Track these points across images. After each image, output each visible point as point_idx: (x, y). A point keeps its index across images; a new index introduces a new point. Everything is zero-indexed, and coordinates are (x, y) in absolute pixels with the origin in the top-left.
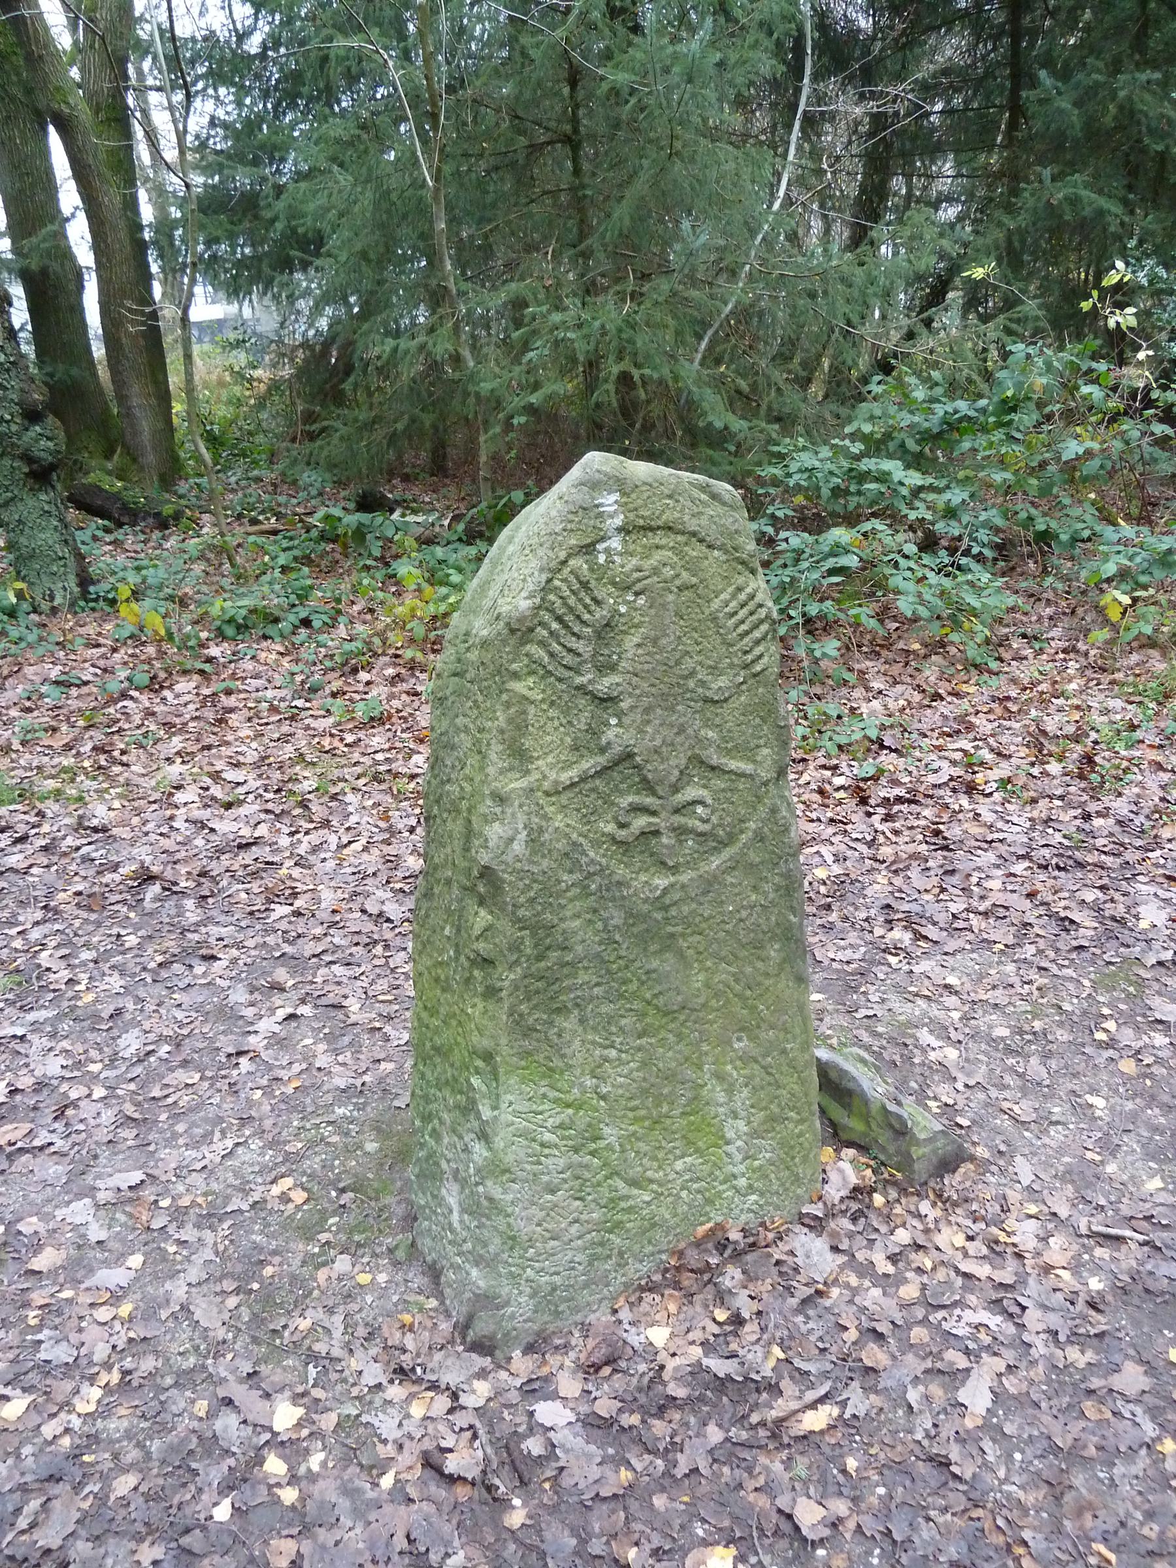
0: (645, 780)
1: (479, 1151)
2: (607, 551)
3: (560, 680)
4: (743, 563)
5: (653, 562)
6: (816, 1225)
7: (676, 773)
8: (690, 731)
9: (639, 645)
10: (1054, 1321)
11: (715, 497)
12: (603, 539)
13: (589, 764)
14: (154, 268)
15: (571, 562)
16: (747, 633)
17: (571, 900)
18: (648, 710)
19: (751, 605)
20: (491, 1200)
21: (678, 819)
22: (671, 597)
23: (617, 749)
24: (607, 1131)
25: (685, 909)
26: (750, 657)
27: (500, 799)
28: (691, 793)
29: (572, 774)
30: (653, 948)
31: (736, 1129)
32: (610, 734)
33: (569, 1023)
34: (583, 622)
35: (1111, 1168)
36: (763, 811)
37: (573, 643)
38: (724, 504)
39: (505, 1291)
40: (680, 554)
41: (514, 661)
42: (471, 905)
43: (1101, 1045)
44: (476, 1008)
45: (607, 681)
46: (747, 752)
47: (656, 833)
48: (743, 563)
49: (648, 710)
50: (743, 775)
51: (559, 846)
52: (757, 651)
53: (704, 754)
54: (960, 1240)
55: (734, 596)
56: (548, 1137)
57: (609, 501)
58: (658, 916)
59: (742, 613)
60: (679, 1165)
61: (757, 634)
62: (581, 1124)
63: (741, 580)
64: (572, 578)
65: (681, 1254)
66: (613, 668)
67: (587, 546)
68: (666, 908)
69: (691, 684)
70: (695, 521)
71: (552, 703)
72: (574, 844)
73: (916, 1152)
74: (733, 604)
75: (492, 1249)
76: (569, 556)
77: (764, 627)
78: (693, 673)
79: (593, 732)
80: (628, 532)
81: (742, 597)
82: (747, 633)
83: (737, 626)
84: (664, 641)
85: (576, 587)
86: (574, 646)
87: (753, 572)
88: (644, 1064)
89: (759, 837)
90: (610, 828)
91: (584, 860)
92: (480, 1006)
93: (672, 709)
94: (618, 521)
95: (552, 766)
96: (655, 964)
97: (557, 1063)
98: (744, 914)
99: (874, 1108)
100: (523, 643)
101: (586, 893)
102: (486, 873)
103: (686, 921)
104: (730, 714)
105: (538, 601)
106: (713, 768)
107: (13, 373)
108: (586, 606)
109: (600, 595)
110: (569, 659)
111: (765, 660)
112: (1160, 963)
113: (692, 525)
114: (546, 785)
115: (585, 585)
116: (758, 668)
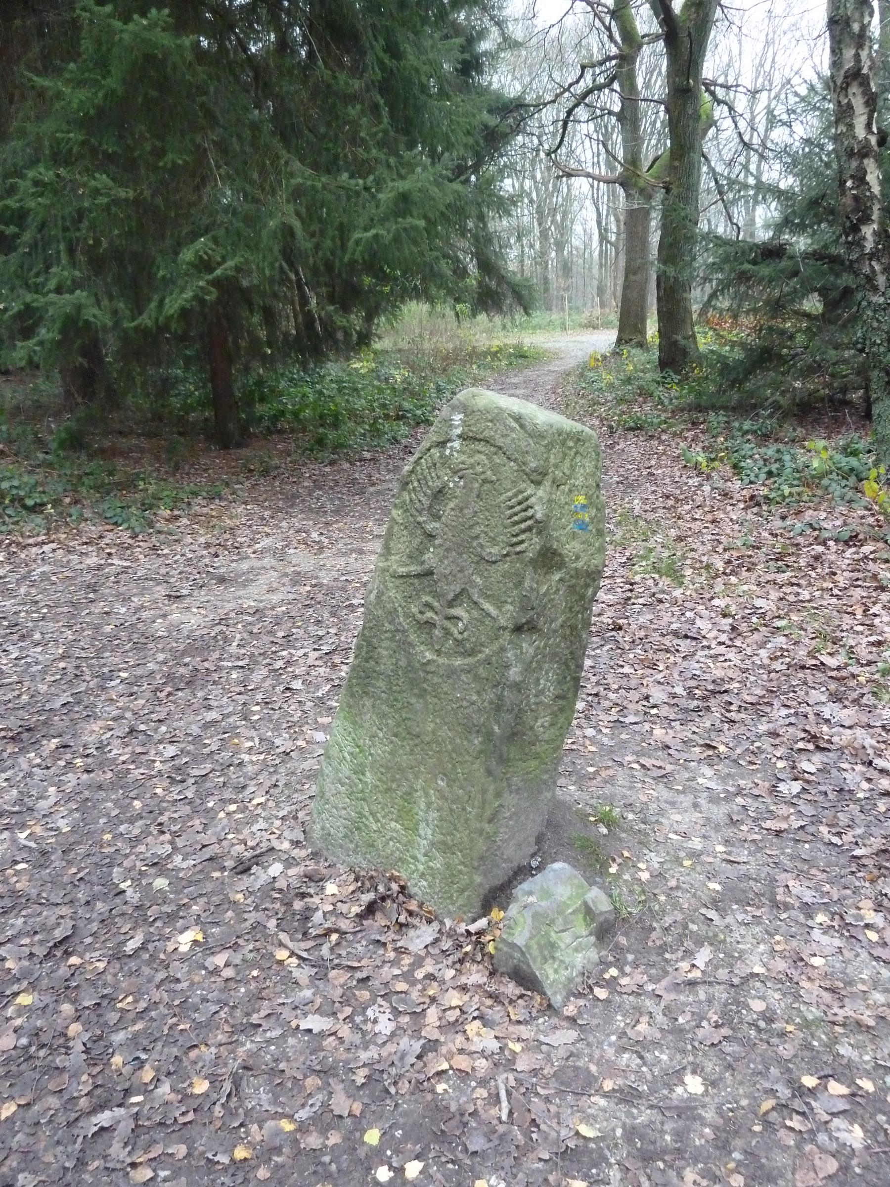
12: (449, 440)
13: (414, 569)
21: (447, 624)
30: (416, 691)
33: (368, 703)
40: (490, 459)
46: (500, 604)
49: (448, 550)
50: (489, 615)
52: (523, 537)
55: (516, 495)
58: (422, 674)
59: (518, 508)
63: (523, 486)
69: (475, 544)
77: (529, 523)
78: (477, 537)
81: (520, 497)
89: (488, 661)
90: (415, 610)
94: (459, 431)
101: (392, 639)
109: (441, 473)
110: (418, 505)
111: (524, 546)
113: (500, 442)
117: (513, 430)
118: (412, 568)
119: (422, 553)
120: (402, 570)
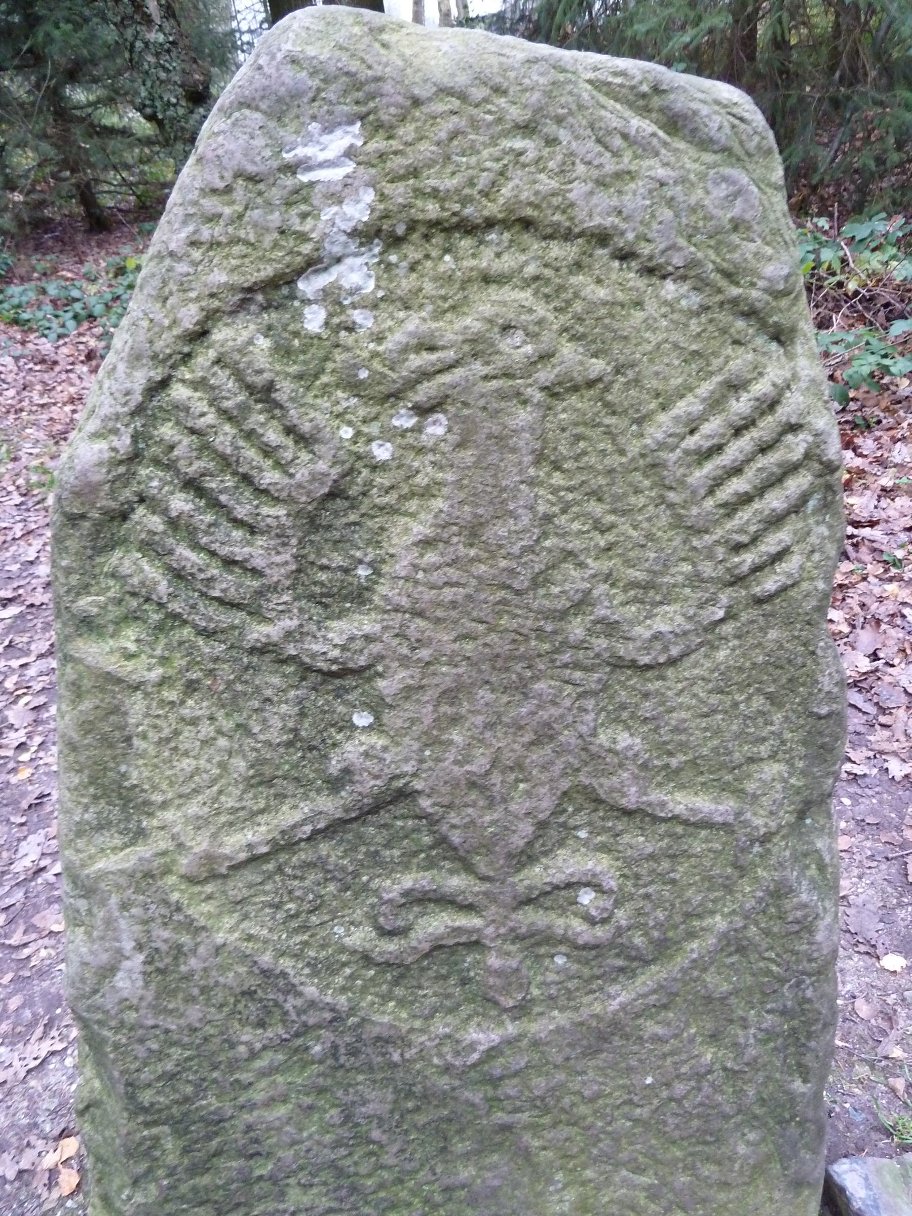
0: (442, 841)
2: (332, 297)
3: (207, 634)
4: (751, 314)
5: (471, 322)
7: (527, 828)
8: (567, 737)
9: (426, 543)
11: (676, 123)
12: (313, 264)
15: (220, 334)
16: (746, 499)
17: (263, 1074)
19: (767, 426)
22: (523, 416)
23: (369, 785)
26: (748, 558)
28: (567, 863)
29: (256, 835)
32: (351, 751)
34: (262, 492)
36: (748, 893)
37: (236, 544)
38: (704, 143)
41: (85, 589)
45: (340, 630)
46: (723, 772)
48: (751, 314)
49: (450, 695)
50: (706, 824)
51: (229, 978)
52: (771, 543)
53: (603, 785)
55: (715, 404)
57: (327, 152)
58: (476, 1096)
59: (735, 451)
61: (775, 501)
63: (739, 361)
64: (223, 379)
66: (360, 597)
67: (272, 284)
69: (576, 629)
70: (604, 200)
71: (191, 687)
72: (266, 973)
74: (713, 426)
76: (211, 317)
77: (796, 484)
79: (309, 745)
80: (395, 241)
81: (741, 405)
82: (746, 499)
83: (717, 483)
84: (500, 530)
85: (235, 399)
86: (240, 552)
87: (781, 336)
89: (735, 944)
90: (360, 937)
91: (291, 1003)
93: (522, 688)
94: (358, 210)
95: (200, 823)
98: (680, 1088)
103: (540, 1104)
104: (683, 694)
105: (123, 443)
106: (628, 813)
107: (174, 54)
108: (268, 451)
110: (227, 583)
111: (792, 564)
113: (596, 210)
115: (264, 394)
116: (770, 584)
117: (640, 146)
118: (289, 815)
119: (317, 749)
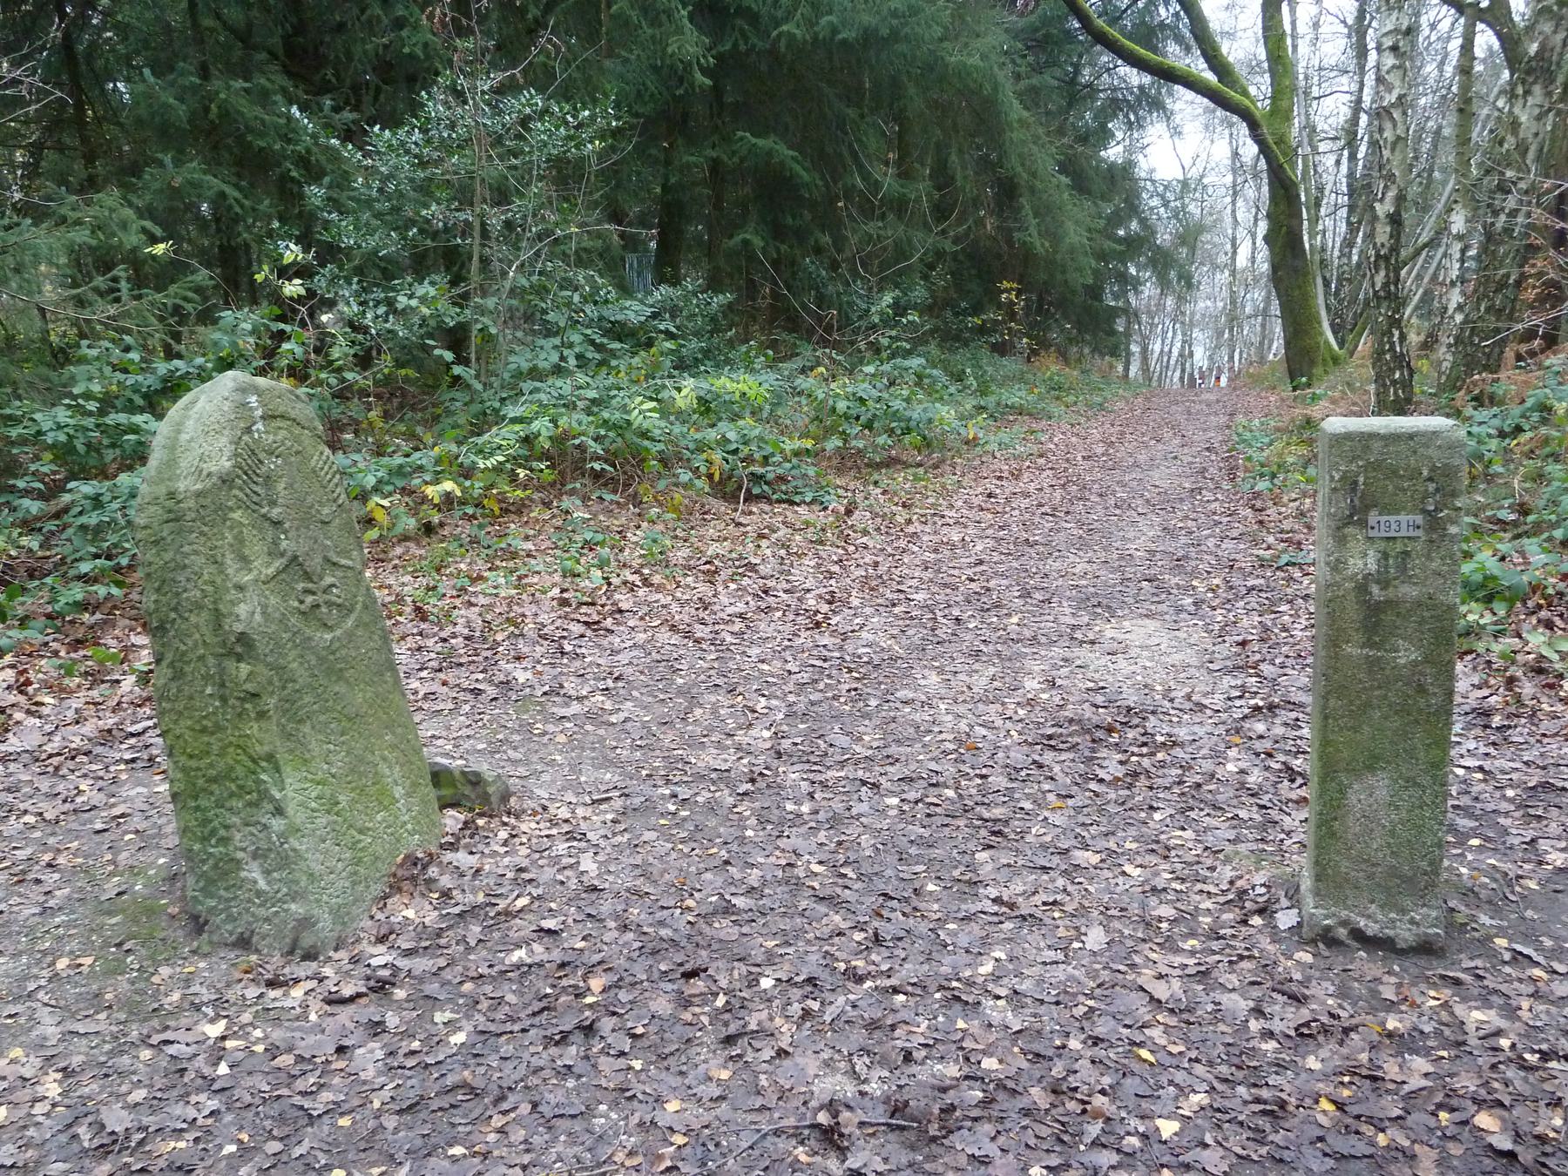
0: (306, 573)
1: (277, 824)
6: (453, 847)
10: (602, 832)
13: (278, 563)
14: (1305, 216)
18: (297, 529)
20: (294, 850)
24: (341, 798)
25: (344, 652)
27: (240, 588)
28: (329, 580)
31: (398, 792)
32: (284, 544)
33: (306, 729)
35: (583, 779)
39: (315, 912)
42: (230, 664)
43: (539, 735)
44: (253, 729)
46: (345, 553)
47: (318, 606)
54: (534, 825)
56: (313, 805)
60: (379, 817)
62: (328, 793)
65: (394, 875)
68: (333, 653)
73: (491, 790)
75: (303, 884)
79: (276, 543)
88: (348, 753)
92: (256, 726)
94: (259, 412)
96: (337, 689)
97: (307, 756)
99: (457, 774)
100: (231, 488)
102: (242, 638)
103: (344, 660)
110: (255, 498)
112: (545, 693)
113: (293, 414)
114: (263, 577)
120: (271, 571)
